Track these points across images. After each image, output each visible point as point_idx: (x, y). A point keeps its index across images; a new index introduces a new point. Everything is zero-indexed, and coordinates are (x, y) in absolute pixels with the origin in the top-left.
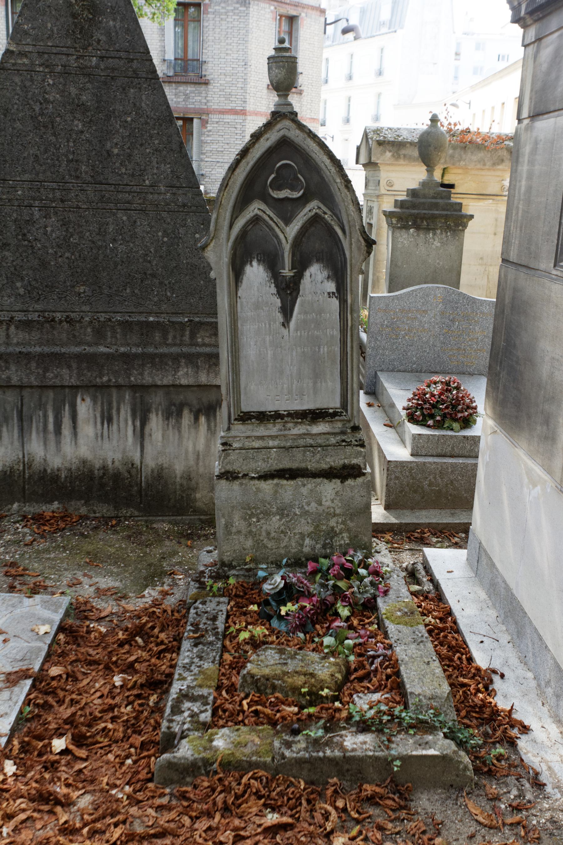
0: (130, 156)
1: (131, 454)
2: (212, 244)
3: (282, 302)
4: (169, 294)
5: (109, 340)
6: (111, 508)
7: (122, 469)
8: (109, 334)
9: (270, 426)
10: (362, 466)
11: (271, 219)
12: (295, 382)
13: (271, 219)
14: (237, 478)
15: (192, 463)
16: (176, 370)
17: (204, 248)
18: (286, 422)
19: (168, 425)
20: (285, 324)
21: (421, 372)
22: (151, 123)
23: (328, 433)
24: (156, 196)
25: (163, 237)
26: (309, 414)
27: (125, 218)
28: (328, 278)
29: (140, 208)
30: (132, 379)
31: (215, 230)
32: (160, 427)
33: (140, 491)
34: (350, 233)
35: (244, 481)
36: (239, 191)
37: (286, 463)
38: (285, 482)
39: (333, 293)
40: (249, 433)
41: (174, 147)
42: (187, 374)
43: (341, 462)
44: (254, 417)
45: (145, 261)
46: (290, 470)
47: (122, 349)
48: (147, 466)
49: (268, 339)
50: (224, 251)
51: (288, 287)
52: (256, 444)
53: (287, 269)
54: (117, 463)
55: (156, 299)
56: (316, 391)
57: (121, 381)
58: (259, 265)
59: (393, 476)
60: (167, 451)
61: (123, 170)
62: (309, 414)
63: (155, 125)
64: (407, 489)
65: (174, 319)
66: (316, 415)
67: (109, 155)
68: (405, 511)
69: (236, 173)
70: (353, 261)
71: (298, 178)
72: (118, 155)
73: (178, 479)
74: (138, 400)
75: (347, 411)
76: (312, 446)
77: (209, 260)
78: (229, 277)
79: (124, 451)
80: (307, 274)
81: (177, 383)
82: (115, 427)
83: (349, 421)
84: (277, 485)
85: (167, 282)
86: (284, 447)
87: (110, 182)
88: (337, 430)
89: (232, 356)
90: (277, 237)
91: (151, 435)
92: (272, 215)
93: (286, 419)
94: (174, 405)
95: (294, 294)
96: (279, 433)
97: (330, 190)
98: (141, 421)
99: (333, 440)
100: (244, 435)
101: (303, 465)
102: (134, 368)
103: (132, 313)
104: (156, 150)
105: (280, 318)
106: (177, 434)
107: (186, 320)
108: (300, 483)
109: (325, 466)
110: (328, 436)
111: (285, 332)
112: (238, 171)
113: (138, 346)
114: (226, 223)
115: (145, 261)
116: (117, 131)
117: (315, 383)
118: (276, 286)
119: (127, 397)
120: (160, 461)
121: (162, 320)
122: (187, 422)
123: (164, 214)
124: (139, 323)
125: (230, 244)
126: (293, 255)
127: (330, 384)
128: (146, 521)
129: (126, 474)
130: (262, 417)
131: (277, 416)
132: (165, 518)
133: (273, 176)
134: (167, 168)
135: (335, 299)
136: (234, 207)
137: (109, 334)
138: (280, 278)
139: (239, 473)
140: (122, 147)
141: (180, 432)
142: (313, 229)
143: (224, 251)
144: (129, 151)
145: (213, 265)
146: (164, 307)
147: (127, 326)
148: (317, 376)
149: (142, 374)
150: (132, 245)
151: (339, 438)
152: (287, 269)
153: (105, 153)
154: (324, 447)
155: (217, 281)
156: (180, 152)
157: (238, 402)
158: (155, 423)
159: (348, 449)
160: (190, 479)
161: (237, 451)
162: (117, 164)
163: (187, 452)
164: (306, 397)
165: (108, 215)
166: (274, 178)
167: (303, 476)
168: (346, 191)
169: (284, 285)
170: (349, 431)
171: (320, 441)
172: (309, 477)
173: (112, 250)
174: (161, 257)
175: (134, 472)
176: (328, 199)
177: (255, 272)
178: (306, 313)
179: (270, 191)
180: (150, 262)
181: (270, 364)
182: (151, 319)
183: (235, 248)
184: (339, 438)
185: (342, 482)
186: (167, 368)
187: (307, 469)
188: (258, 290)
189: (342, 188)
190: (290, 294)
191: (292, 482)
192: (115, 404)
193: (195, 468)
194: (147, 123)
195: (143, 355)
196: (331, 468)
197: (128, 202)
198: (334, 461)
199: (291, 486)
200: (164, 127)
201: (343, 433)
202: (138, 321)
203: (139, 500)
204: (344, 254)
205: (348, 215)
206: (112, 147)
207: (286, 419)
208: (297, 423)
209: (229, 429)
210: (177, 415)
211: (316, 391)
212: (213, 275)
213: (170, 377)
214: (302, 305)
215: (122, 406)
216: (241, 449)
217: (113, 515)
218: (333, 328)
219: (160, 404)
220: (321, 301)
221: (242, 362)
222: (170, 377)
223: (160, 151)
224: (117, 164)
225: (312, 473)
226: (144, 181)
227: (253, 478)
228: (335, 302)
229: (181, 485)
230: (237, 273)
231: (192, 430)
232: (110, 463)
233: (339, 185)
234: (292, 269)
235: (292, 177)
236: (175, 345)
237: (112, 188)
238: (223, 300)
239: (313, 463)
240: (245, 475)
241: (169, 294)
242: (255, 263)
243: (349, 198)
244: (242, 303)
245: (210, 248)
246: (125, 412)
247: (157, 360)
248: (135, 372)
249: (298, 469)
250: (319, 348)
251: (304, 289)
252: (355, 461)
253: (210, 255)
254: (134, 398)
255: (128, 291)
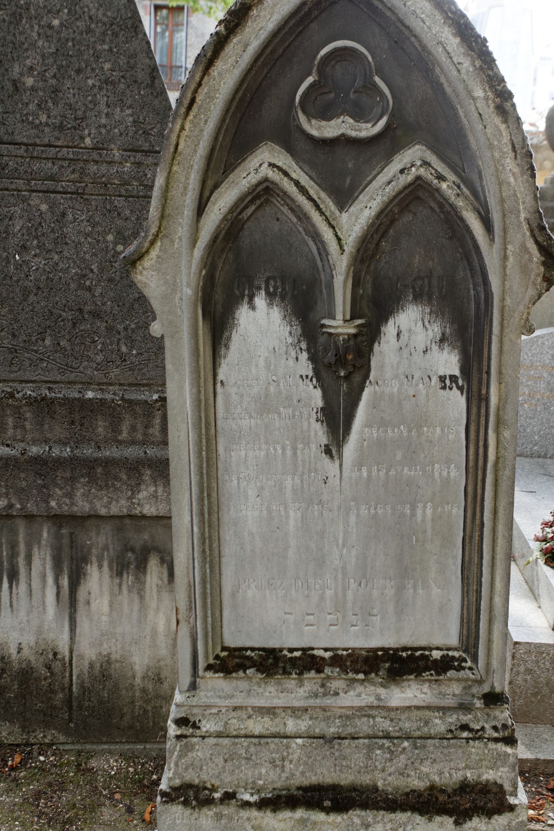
0: (56, 91)
1: (52, 636)
2: (154, 253)
3: (325, 396)
4: (124, 349)
5: (10, 432)
6: (17, 729)
7: (37, 662)
8: (10, 421)
9: (291, 683)
10: (507, 787)
11: (303, 190)
12: (353, 585)
13: (303, 190)
14: (209, 802)
15: (164, 652)
16: (135, 489)
17: (134, 261)
18: (328, 678)
19: (120, 585)
20: (333, 449)
21: (545, 457)
22: (98, 31)
23: (428, 708)
24: (104, 168)
25: (116, 244)
26: (383, 659)
27: (44, 207)
28: (443, 340)
29: (72, 188)
30: (53, 504)
31: (162, 217)
32: (106, 589)
33: (69, 701)
34: (505, 231)
35: (226, 810)
36: (223, 120)
37: (325, 773)
38: (321, 816)
39: (453, 378)
40: (238, 701)
41: (141, 76)
42: (155, 496)
43: (458, 776)
44: (253, 664)
45: (81, 286)
46: (335, 788)
47: (34, 450)
48: (81, 657)
49: (289, 483)
50: (184, 271)
51: (340, 361)
52: (257, 726)
53: (339, 316)
54: (26, 652)
55: (99, 358)
56: (401, 607)
57: (31, 507)
58: (270, 304)
59: (522, 669)
60: (119, 630)
61: (44, 118)
62: (383, 659)
63: (104, 34)
64: (546, 690)
65: (133, 396)
66: (400, 664)
67: (17, 89)
68: (541, 728)
69: (215, 71)
70: (508, 301)
71: (375, 86)
72: (33, 89)
73: (138, 681)
74: (66, 541)
75: (475, 659)
76: (387, 736)
77: (147, 292)
78: (195, 335)
79: (40, 631)
80: (389, 330)
81: (137, 511)
82: (23, 587)
83: (480, 682)
84: (303, 821)
85: (120, 327)
86: (322, 737)
87: (18, 139)
88: (450, 702)
89: (202, 522)
90: (316, 236)
91: (88, 603)
92: (304, 180)
93: (328, 670)
94: (132, 550)
95: (357, 378)
96: (312, 702)
97: (456, 115)
98: (70, 578)
99: (439, 725)
100: (227, 702)
101: (366, 779)
102: (57, 485)
103: (56, 382)
104: (106, 82)
105: (319, 434)
106: (137, 601)
107: (155, 397)
108: (357, 821)
109: (417, 783)
110: (427, 713)
111: (331, 467)
112: (220, 65)
113: (65, 444)
114: (189, 200)
115: (81, 286)
116: (34, 45)
117: (400, 589)
118: (313, 359)
119: (45, 535)
120: (105, 649)
121: (109, 397)
122: (155, 580)
123: (119, 202)
124: (67, 402)
125: (198, 252)
126: (356, 284)
127: (436, 591)
128: (79, 753)
129: (44, 672)
130: (271, 663)
131: (307, 662)
132: (113, 747)
133: (310, 80)
134: (126, 116)
135: (456, 392)
136: (210, 158)
137: (10, 421)
138: (322, 340)
139: (214, 789)
140: (42, 74)
141: (142, 598)
142: (408, 218)
143: (184, 271)
144: (54, 82)
145: (155, 304)
146: (114, 373)
147: (44, 407)
148: (405, 572)
149: (70, 495)
150: (56, 257)
151: (453, 719)
152: (339, 316)
153: (9, 85)
154: (418, 739)
155: (167, 343)
156: (152, 85)
157: (215, 627)
158: (97, 582)
159: (475, 747)
160: (159, 680)
161: (212, 741)
162: (32, 107)
163: (154, 633)
164: (377, 620)
165: (12, 200)
166: (312, 86)
167: (364, 806)
168: (497, 120)
169: (330, 357)
170: (479, 704)
171: (408, 725)
172: (378, 808)
173: (18, 266)
174: (111, 280)
175: (57, 666)
176: (451, 143)
177: (261, 324)
178: (383, 424)
179: (302, 118)
180: (89, 289)
181: (293, 543)
182: (90, 395)
183: (210, 263)
184: (453, 719)
185: (457, 823)
186: (118, 485)
187: (375, 789)
188: (268, 367)
189: (489, 111)
190: (347, 378)
191: (337, 818)
192: (22, 547)
193: (169, 661)
194: (89, 31)
195: (73, 461)
196: (432, 787)
197: (52, 178)
198: (441, 773)
199: (338, 825)
200: (121, 38)
201: (464, 707)
202: (65, 399)
203: (66, 716)
204: (486, 283)
205: (500, 184)
206: (22, 74)
207: (328, 670)
208: (355, 680)
209: (193, 686)
210: (138, 568)
211: (401, 607)
212: (156, 329)
213: (123, 502)
214: (374, 405)
215: (35, 550)
216: (219, 735)
217: (19, 741)
218: (448, 462)
219: (106, 548)
220: (422, 398)
221: (228, 535)
222: (123, 502)
223: (113, 83)
224: (32, 107)
225: (386, 800)
226: (82, 138)
227: (247, 804)
228: (457, 402)
229: (144, 691)
230: (217, 322)
231: (165, 595)
232: (13, 651)
233: (481, 104)
234: (353, 318)
235: (359, 83)
236: (133, 442)
237: (22, 151)
238: (181, 388)
239: (390, 773)
240: (229, 797)
241: (124, 349)
242: (260, 301)
243: (506, 139)
244: (227, 396)
245: (147, 262)
246: (42, 561)
247: (99, 470)
248: (59, 492)
249: (353, 788)
250: (413, 509)
251: (382, 367)
252: (489, 775)
253: (149, 278)
254: (58, 537)
255: (48, 342)
